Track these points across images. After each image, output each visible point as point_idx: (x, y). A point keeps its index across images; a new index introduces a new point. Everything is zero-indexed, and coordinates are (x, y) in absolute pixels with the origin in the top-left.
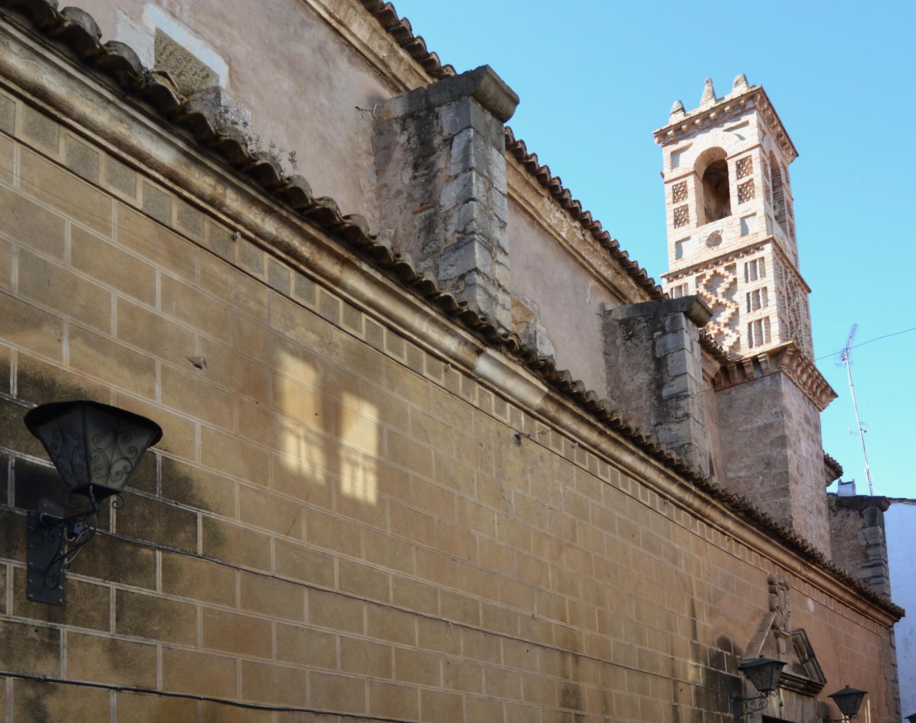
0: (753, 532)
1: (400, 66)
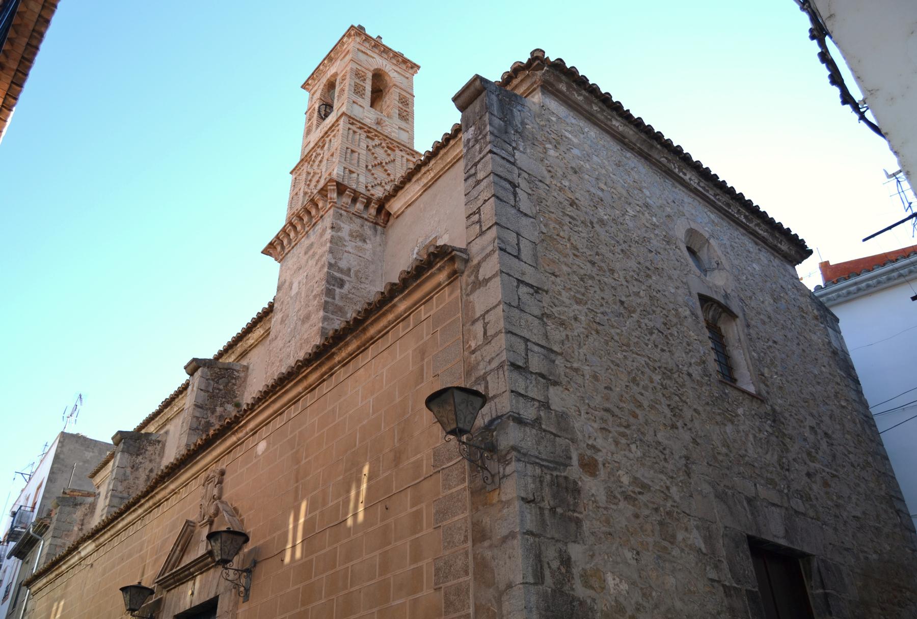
0: (202, 458)
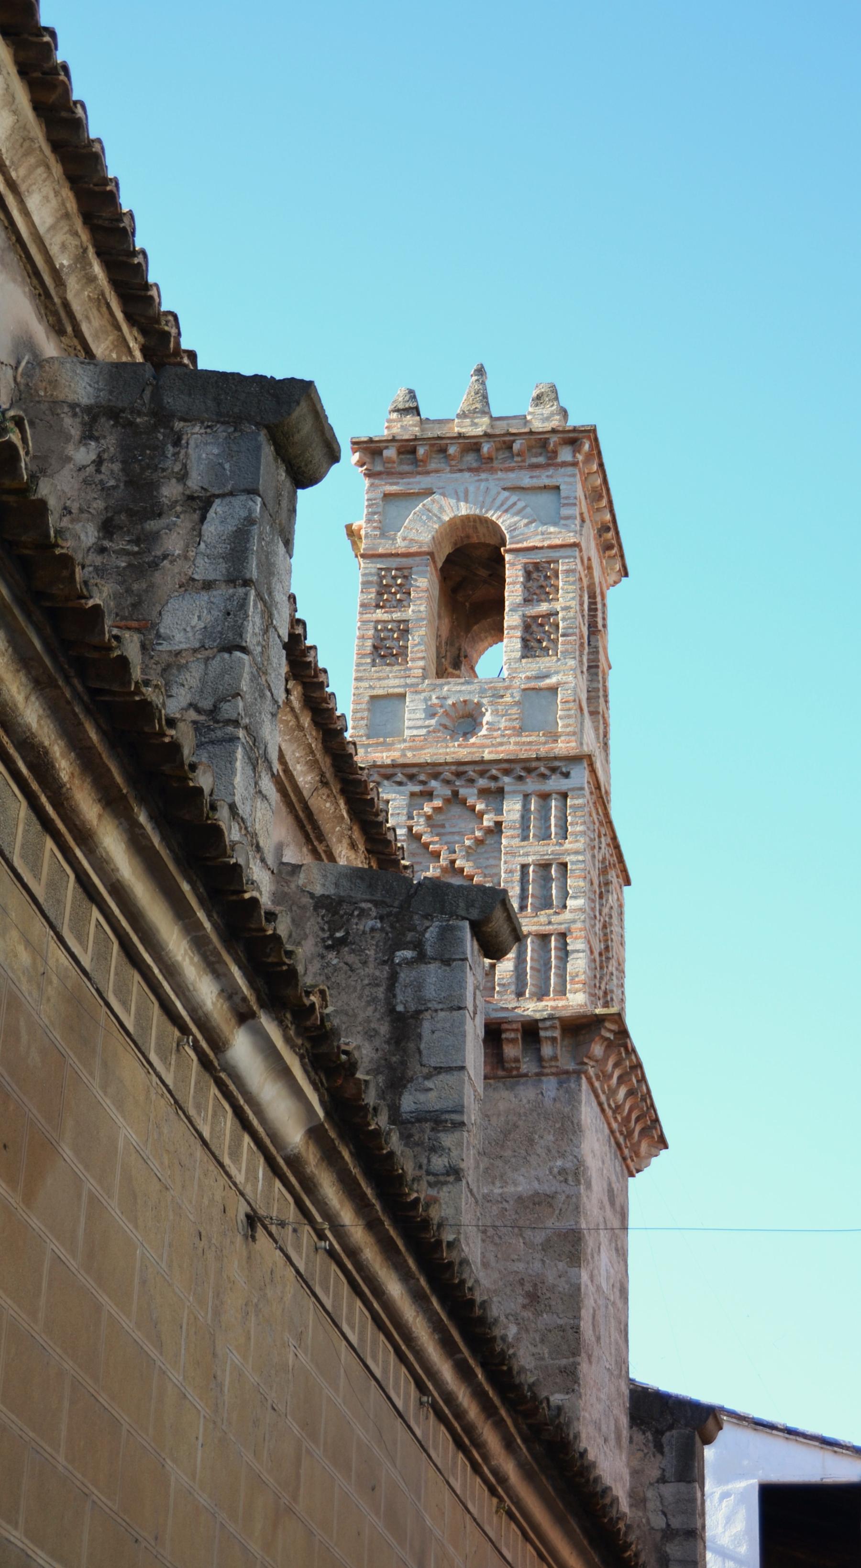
1: (83, 289)
